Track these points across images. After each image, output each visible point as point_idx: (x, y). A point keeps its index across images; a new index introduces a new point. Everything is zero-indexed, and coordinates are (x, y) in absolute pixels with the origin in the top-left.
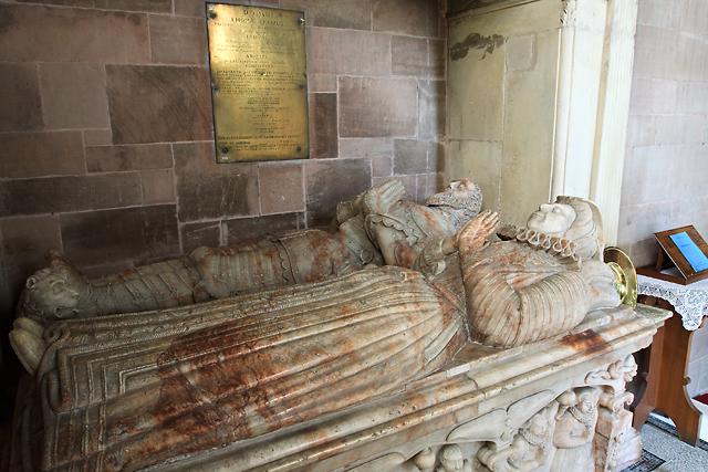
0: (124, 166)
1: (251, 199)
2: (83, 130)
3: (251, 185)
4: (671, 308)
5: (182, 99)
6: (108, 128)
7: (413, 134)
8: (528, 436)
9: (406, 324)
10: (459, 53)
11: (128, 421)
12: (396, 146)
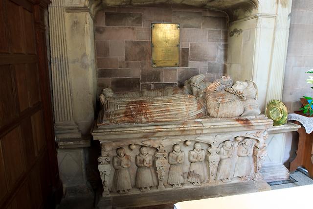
0: (127, 67)
1: (161, 78)
2: (118, 57)
3: (161, 74)
4: (301, 125)
5: (144, 49)
6: (124, 57)
7: (215, 61)
8: (225, 147)
9: (184, 107)
10: (232, 35)
11: (119, 114)
12: (209, 64)
